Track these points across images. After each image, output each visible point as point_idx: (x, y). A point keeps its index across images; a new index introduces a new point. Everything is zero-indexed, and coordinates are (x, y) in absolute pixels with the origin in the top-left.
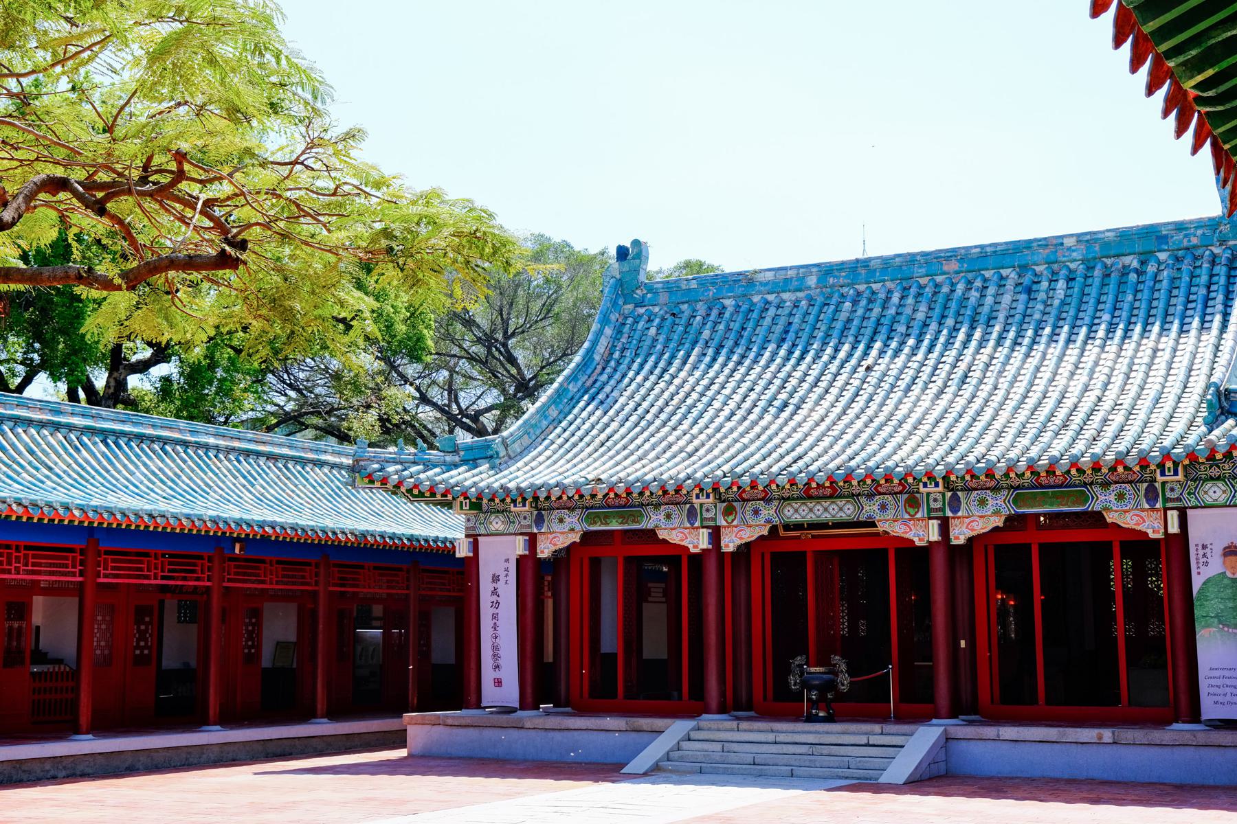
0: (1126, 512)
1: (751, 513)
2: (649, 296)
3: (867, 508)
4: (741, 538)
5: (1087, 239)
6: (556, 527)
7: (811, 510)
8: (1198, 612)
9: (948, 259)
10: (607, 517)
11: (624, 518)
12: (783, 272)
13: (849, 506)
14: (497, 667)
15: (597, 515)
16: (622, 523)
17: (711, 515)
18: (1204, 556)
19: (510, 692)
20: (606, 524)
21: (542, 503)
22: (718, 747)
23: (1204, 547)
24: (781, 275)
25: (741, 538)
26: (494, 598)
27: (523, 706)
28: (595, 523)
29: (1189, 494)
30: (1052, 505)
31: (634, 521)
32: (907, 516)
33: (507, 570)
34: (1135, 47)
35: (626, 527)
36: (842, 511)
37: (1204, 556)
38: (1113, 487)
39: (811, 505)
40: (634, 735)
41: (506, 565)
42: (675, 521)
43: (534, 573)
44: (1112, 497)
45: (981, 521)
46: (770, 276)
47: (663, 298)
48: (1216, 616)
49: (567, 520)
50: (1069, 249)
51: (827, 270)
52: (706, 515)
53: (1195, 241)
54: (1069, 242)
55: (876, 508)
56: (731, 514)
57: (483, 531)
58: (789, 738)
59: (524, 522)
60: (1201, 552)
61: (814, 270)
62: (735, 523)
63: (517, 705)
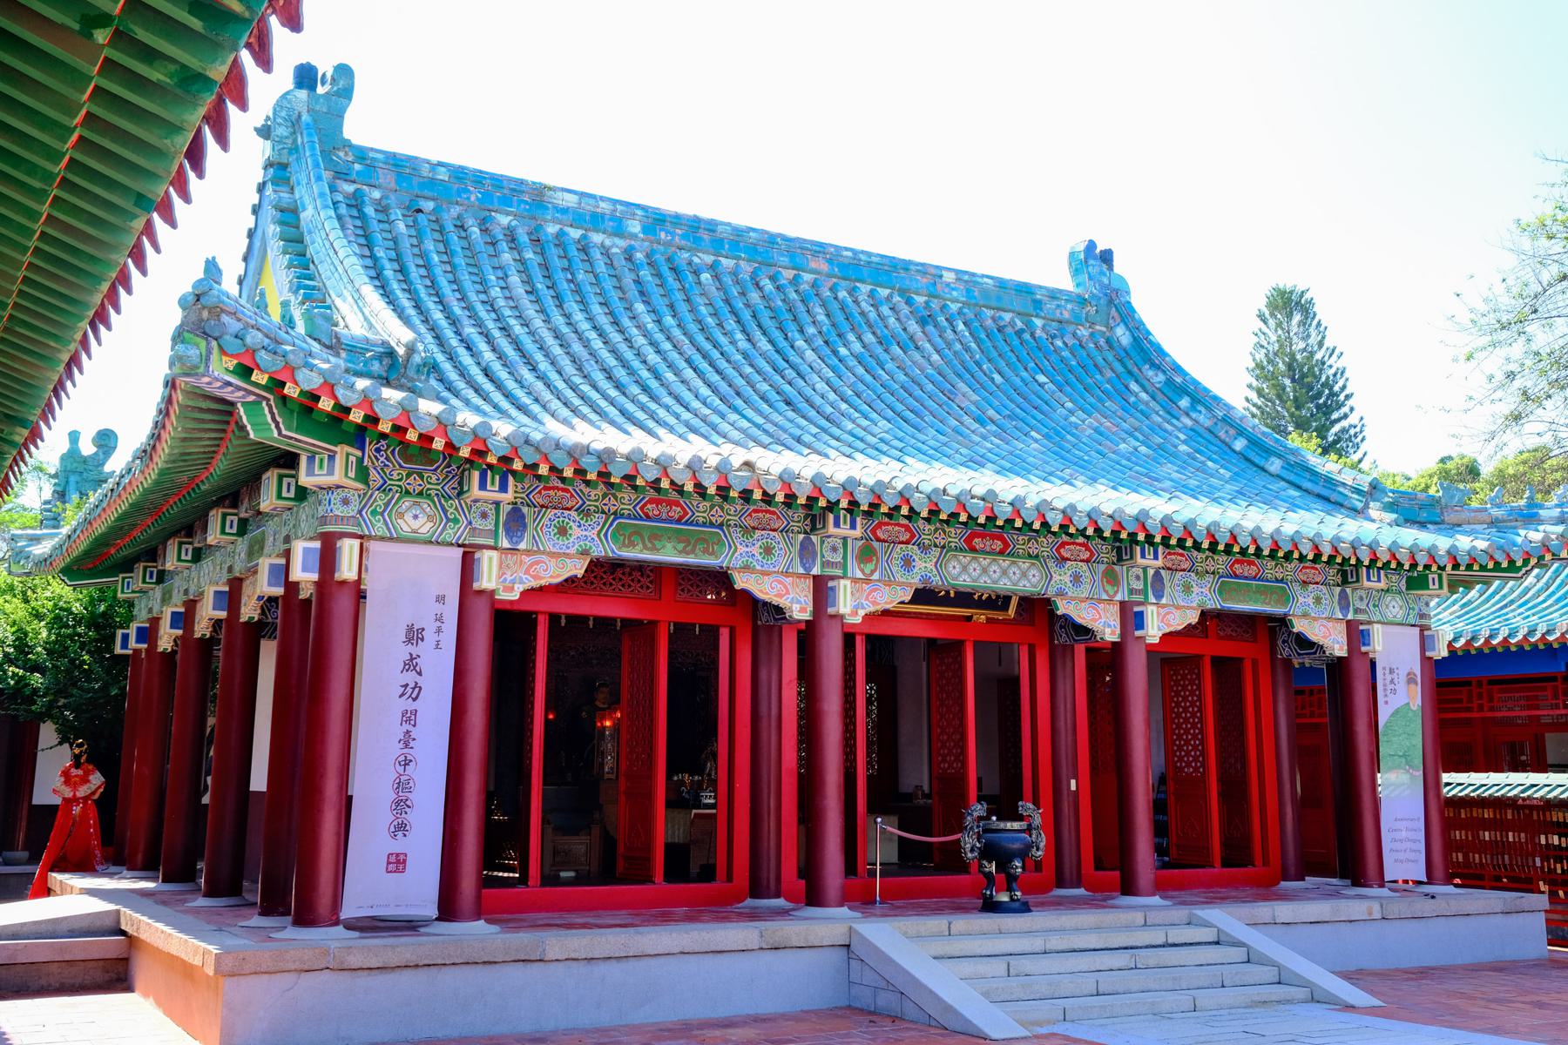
0: (768, 574)
1: (1181, 588)
2: (357, 167)
3: (1056, 577)
4: (875, 603)
5: (967, 280)
6: (550, 542)
7: (985, 570)
8: (1384, 750)
9: (815, 254)
10: (655, 537)
11: (688, 543)
12: (592, 201)
13: (1033, 571)
14: (402, 828)
15: (637, 532)
16: (684, 552)
17: (838, 558)
18: (1392, 681)
19: (418, 890)
20: (654, 549)
21: (551, 483)
22: (999, 967)
23: (1392, 671)
24: (588, 206)
25: (875, 603)
26: (410, 677)
27: (448, 909)
28: (632, 544)
29: (374, 513)
30: (1256, 601)
31: (705, 551)
32: (1105, 597)
33: (439, 619)
34: (234, 101)
35: (691, 560)
36: (1014, 577)
37: (1392, 681)
38: (758, 533)
39: (985, 563)
40: (769, 957)
41: (438, 608)
42: (780, 560)
43: (507, 639)
44: (1310, 601)
45: (1177, 613)
46: (571, 200)
47: (386, 178)
48: (1404, 756)
49: (575, 531)
50: (948, 284)
51: (657, 220)
52: (829, 557)
53: (1066, 315)
54: (949, 277)
55: (1067, 579)
56: (870, 560)
57: (379, 528)
58: (1093, 941)
59: (478, 523)
60: (1389, 677)
61: (639, 212)
62: (876, 576)
63: (432, 911)
